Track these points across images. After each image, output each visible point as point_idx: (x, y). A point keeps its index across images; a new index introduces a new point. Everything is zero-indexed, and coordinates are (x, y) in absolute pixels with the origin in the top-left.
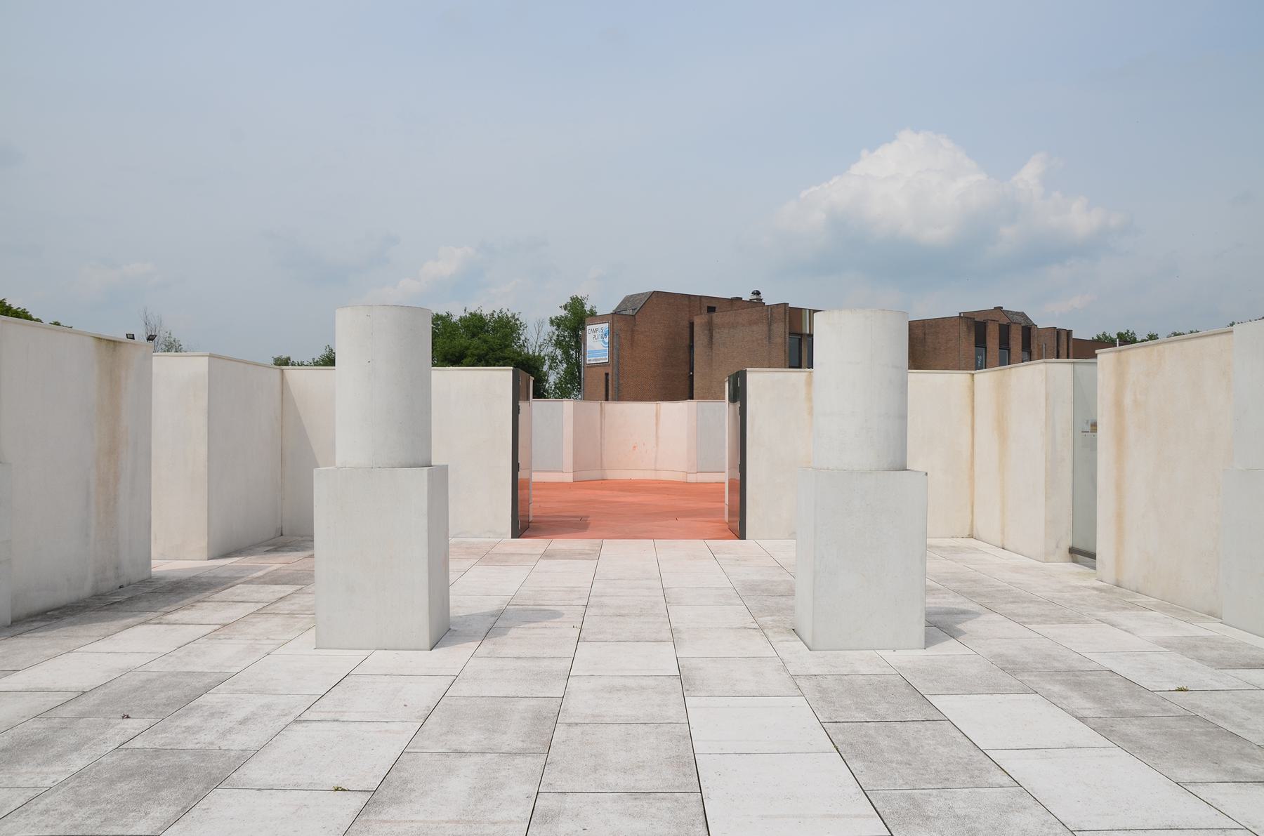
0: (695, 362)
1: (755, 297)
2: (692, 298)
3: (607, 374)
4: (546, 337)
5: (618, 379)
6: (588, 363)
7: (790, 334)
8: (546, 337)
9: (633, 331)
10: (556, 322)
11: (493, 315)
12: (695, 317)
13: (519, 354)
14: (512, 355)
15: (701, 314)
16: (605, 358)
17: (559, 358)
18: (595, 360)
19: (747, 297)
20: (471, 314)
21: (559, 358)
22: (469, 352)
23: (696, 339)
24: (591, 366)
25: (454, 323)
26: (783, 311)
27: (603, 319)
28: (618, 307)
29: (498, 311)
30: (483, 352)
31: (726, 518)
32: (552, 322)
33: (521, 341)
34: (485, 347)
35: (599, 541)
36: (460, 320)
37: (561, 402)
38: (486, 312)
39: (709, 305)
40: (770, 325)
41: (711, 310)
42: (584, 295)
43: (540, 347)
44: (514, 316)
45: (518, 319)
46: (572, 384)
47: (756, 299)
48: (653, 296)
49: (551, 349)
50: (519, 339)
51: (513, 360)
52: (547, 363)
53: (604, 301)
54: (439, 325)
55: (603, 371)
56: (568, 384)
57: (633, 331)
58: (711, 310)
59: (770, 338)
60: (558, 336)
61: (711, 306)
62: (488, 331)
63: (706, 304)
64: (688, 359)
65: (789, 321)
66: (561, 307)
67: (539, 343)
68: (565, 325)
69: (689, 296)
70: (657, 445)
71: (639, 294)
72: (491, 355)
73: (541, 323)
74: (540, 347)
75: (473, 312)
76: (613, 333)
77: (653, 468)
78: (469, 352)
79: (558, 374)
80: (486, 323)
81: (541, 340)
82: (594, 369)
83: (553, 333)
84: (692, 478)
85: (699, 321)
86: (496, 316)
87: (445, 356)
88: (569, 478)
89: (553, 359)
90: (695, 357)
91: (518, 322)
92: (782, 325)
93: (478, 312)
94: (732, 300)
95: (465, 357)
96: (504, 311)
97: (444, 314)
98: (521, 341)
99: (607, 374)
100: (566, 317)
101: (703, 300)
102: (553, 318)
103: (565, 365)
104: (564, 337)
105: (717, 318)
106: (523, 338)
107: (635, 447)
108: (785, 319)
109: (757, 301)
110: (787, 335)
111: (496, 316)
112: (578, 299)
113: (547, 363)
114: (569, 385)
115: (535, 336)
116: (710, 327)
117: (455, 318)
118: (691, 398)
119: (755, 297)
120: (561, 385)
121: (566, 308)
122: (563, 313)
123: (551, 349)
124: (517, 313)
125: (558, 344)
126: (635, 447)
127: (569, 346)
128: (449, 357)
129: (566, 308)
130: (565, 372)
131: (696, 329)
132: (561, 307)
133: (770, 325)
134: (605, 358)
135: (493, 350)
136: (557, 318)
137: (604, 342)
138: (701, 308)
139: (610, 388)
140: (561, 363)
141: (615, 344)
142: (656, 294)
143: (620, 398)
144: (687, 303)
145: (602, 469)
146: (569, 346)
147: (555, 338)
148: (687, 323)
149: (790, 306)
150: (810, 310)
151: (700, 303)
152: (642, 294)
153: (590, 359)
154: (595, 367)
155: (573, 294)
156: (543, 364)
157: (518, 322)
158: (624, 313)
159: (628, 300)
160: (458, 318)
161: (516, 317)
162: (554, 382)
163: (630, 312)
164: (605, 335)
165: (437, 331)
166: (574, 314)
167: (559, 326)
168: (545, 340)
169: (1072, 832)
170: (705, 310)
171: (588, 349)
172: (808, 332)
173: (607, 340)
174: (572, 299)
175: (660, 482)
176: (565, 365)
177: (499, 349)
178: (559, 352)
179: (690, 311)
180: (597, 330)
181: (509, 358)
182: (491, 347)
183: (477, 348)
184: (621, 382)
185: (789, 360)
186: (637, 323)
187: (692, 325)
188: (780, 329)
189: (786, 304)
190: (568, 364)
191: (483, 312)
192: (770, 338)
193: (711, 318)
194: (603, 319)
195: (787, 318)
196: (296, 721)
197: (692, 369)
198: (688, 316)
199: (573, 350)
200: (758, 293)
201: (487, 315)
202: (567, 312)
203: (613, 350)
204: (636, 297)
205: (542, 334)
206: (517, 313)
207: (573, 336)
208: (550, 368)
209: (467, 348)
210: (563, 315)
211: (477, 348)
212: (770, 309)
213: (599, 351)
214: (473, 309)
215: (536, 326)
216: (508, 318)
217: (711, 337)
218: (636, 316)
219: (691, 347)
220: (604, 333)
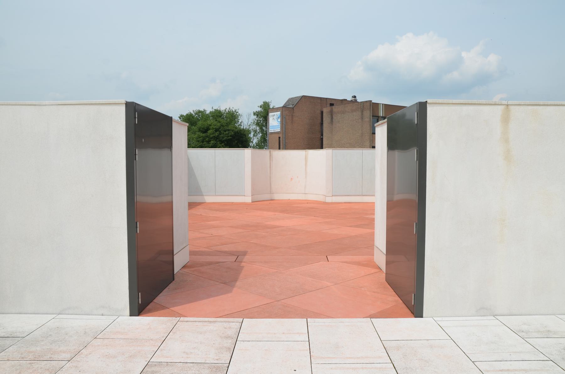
0: (324, 131)
1: (353, 99)
2: (322, 99)
3: (279, 138)
4: (252, 121)
5: (285, 140)
6: (270, 132)
7: (373, 116)
8: (252, 121)
9: (292, 116)
10: (257, 114)
11: (225, 110)
12: (324, 108)
13: (236, 128)
14: (232, 129)
15: (327, 107)
16: (278, 130)
17: (258, 131)
18: (274, 130)
19: (349, 98)
20: (215, 110)
21: (258, 131)
22: (211, 127)
23: (324, 119)
24: (272, 133)
25: (207, 114)
26: (369, 105)
27: (276, 110)
28: (285, 104)
29: (228, 108)
30: (218, 127)
31: (380, 258)
32: (254, 114)
33: (239, 123)
34: (219, 124)
35: (234, 323)
36: (210, 113)
37: (243, 150)
38: (222, 109)
39: (331, 103)
40: (362, 112)
41: (332, 105)
42: (269, 101)
43: (249, 126)
44: (236, 111)
45: (238, 112)
46: (263, 144)
47: (354, 100)
48: (303, 98)
49: (254, 127)
50: (238, 122)
51: (233, 131)
52: (252, 134)
53: (278, 101)
54: (200, 115)
55: (277, 136)
56: (262, 143)
57: (292, 116)
58: (332, 105)
59: (362, 118)
60: (257, 120)
61: (332, 103)
62: (223, 118)
63: (329, 103)
64: (320, 130)
65: (372, 110)
66: (258, 107)
67: (249, 124)
68: (261, 115)
69: (321, 98)
70: (306, 177)
71: (295, 97)
72: (222, 128)
73: (249, 115)
74: (249, 126)
75: (216, 109)
76: (282, 117)
77: (308, 342)
78: (211, 127)
79: (257, 138)
80: (223, 114)
81: (250, 123)
82: (273, 135)
83: (255, 119)
84: (329, 200)
85: (326, 110)
86: (227, 111)
87: (199, 129)
88: (248, 200)
89: (255, 131)
90: (324, 128)
91: (238, 114)
92: (368, 112)
93: (219, 109)
94: (342, 100)
95: (209, 130)
96: (231, 108)
97: (202, 110)
98: (239, 123)
99: (279, 138)
100: (261, 111)
101: (328, 100)
102: (255, 112)
103: (261, 134)
104: (260, 121)
105: (335, 109)
106: (240, 121)
107: (292, 179)
108: (370, 108)
109: (354, 100)
110: (371, 117)
111: (227, 111)
112: (267, 102)
113: (252, 134)
114: (263, 144)
115: (247, 121)
116: (331, 113)
117: (208, 112)
118: (322, 147)
119: (353, 99)
120: (259, 144)
121: (261, 107)
122: (259, 109)
123: (254, 127)
124: (237, 109)
125: (258, 124)
126: (292, 179)
127: (263, 125)
128: (201, 129)
129: (261, 107)
130: (261, 138)
131: (324, 114)
132: (258, 107)
133: (362, 112)
134: (278, 130)
135: (223, 126)
136: (257, 112)
137: (278, 121)
138: (326, 104)
139: (281, 144)
140: (259, 133)
141: (283, 122)
142: (304, 98)
143: (286, 148)
144: (320, 102)
145: (271, 193)
146: (263, 125)
147: (256, 121)
148: (320, 111)
149: (373, 102)
150: (383, 104)
151: (326, 102)
152: (297, 97)
153: (271, 130)
154: (273, 134)
155: (264, 100)
156: (250, 133)
157: (238, 114)
158: (288, 106)
159: (290, 100)
160: (209, 112)
161: (237, 111)
162: (256, 142)
163: (291, 106)
164: (279, 118)
165: (199, 118)
166: (265, 110)
167: (257, 116)
168: (251, 122)
169: (473, 362)
170: (328, 105)
171: (270, 125)
172: (382, 115)
173: (279, 120)
174: (264, 102)
175: (308, 202)
176: (261, 134)
177: (226, 125)
178: (258, 128)
179: (321, 106)
180: (274, 115)
181: (231, 130)
182: (222, 125)
183: (215, 125)
184: (287, 141)
185: (372, 130)
186: (294, 112)
187: (322, 113)
188: (368, 114)
189: (371, 101)
190: (262, 134)
191: (221, 109)
192: (362, 118)
193: (332, 108)
194: (276, 110)
195: (371, 107)
196: (69, 361)
197: (322, 135)
198: (320, 108)
199: (264, 127)
200: (355, 97)
201: (223, 110)
202: (261, 109)
203: (282, 125)
204: (294, 99)
205: (250, 120)
206: (237, 109)
207: (264, 121)
208: (254, 135)
209: (210, 125)
210: (260, 110)
211: (215, 125)
212: (362, 104)
213: (275, 126)
214: (216, 108)
215: (248, 116)
216: (233, 111)
217: (332, 118)
218: (294, 108)
219: (322, 124)
220: (278, 116)
